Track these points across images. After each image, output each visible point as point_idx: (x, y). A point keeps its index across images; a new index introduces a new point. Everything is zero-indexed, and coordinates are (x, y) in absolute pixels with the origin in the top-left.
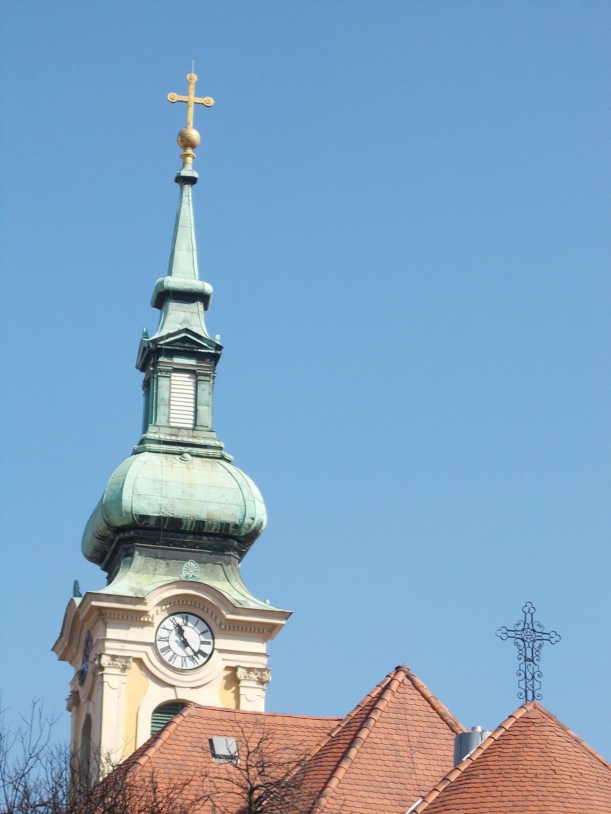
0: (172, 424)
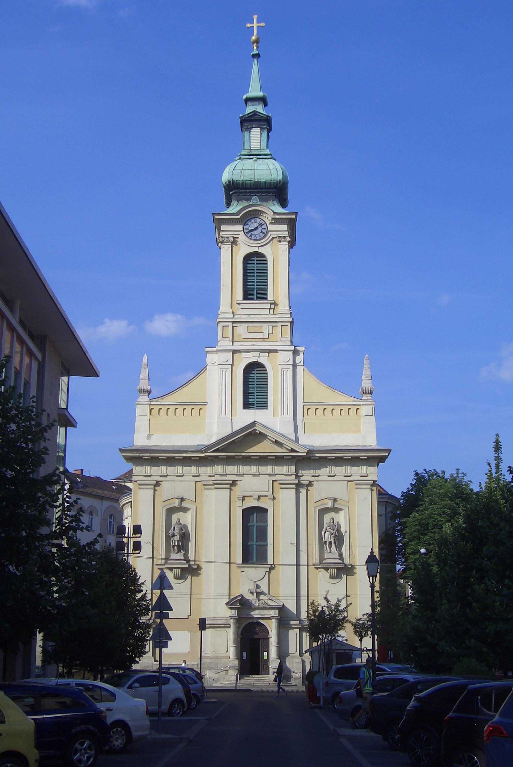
0: (251, 148)
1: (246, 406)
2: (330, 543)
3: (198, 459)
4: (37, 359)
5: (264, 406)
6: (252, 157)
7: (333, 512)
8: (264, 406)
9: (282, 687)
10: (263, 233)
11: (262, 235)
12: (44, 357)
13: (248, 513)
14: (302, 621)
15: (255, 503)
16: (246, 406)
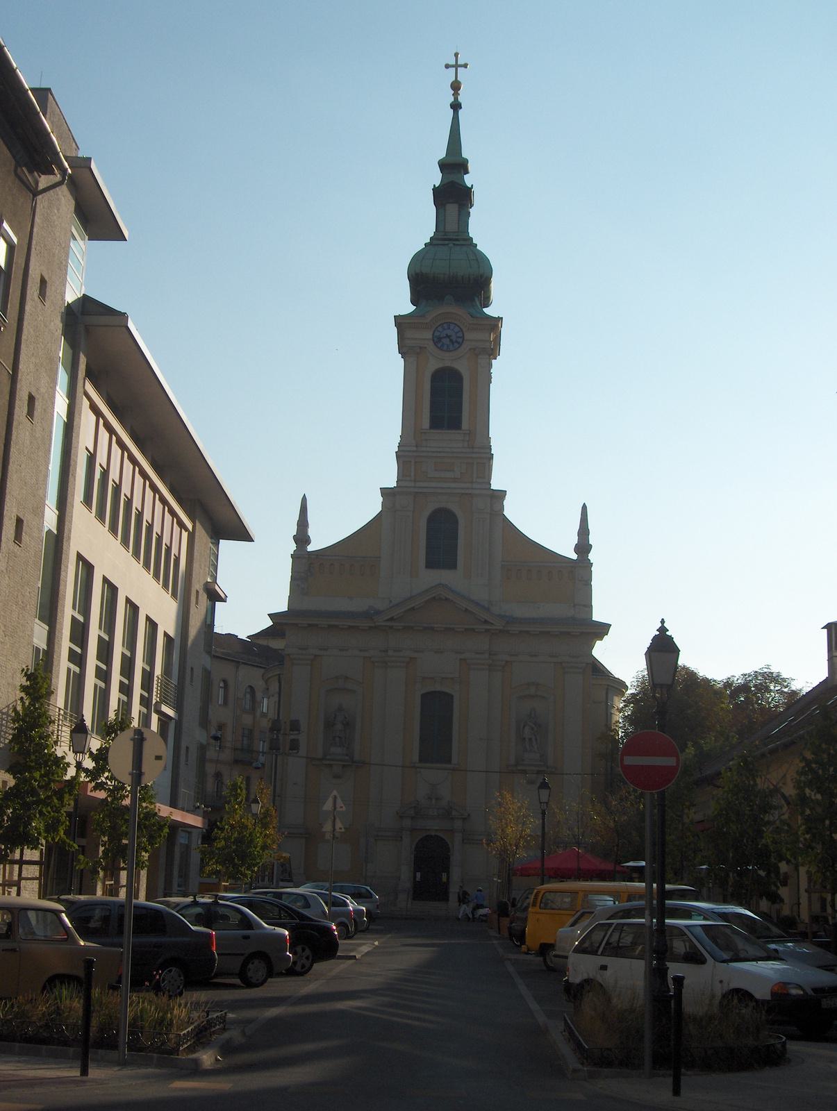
1: (430, 564)
2: (530, 739)
3: (55, 165)
4: (186, 529)
5: (453, 565)
6: (447, 242)
7: (505, 513)
8: (453, 565)
9: (547, 958)
10: (458, 343)
11: (452, 327)
12: (194, 527)
13: (428, 698)
14: (104, 320)
15: (438, 688)
16: (430, 564)
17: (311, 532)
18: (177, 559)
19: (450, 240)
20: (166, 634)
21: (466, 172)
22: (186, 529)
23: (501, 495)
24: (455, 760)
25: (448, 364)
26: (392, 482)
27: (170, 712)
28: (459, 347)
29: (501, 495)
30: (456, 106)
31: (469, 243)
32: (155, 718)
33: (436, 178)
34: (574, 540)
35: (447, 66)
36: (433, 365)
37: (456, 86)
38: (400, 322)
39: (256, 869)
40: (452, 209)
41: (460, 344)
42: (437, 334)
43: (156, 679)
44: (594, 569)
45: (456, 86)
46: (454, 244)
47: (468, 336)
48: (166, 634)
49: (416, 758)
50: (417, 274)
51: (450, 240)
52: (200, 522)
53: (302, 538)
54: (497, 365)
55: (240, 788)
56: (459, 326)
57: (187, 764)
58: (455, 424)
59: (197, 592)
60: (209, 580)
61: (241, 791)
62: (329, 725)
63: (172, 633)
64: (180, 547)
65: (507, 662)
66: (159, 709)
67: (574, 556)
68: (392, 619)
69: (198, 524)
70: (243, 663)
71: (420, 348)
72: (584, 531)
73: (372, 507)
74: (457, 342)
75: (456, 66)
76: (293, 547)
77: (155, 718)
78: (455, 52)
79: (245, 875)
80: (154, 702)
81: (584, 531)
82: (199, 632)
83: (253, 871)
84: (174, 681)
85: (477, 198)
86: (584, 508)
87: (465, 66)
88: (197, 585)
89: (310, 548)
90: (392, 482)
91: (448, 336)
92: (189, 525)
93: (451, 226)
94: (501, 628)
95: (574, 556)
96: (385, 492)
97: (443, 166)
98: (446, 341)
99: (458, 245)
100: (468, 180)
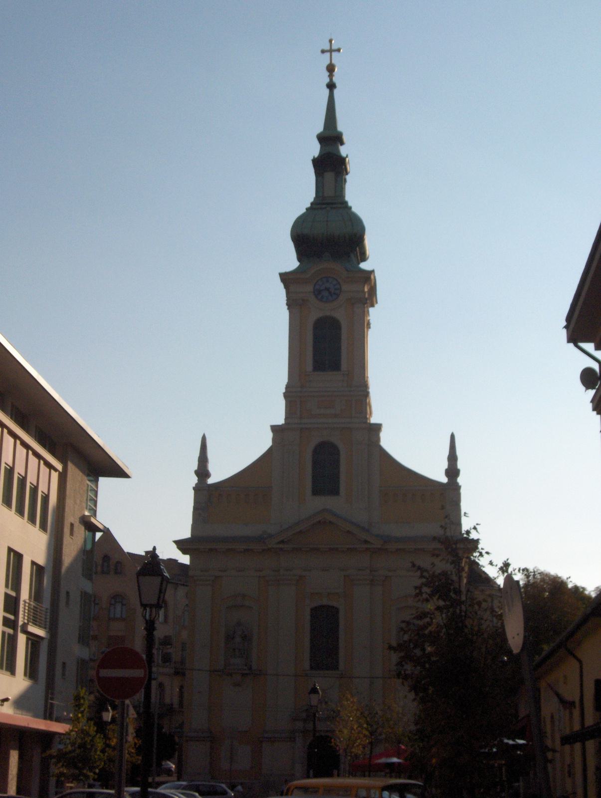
1: (316, 492)
4: (56, 470)
5: (335, 492)
6: (324, 206)
8: (335, 492)
15: (325, 602)
16: (316, 492)
17: (211, 467)
18: (46, 498)
19: (328, 204)
20: (33, 563)
21: (342, 143)
22: (56, 470)
23: (378, 428)
24: (341, 666)
25: (328, 314)
26: (280, 420)
27: (40, 632)
28: (337, 298)
29: (378, 428)
30: (331, 86)
31: (345, 206)
32: (22, 639)
33: (315, 149)
34: (445, 465)
35: (323, 52)
36: (314, 316)
37: (331, 69)
38: (286, 278)
39: (97, 771)
40: (329, 176)
41: (338, 295)
42: (317, 287)
43: (22, 603)
44: (462, 491)
45: (331, 69)
46: (331, 208)
47: (345, 287)
48: (33, 563)
49: (307, 665)
50: (298, 236)
51: (328, 204)
52: (73, 462)
53: (202, 472)
54: (374, 314)
55: (83, 698)
56: (318, 281)
57: (65, 679)
58: (335, 366)
59: (72, 525)
60: (87, 513)
61: (84, 701)
62: (229, 638)
63: (41, 561)
64: (48, 483)
65: (386, 577)
66: (25, 630)
67: (444, 480)
68: (282, 542)
69: (70, 466)
70: (181, 585)
71: (303, 300)
72: (453, 458)
73: (264, 442)
74: (335, 294)
75: (331, 51)
76: (195, 480)
77: (22, 639)
78: (330, 38)
79: (87, 777)
80: (20, 623)
81: (453, 458)
82: (76, 560)
83: (95, 773)
84: (46, 604)
85: (351, 166)
86: (453, 437)
87: (339, 50)
88: (71, 517)
89: (210, 481)
90: (280, 420)
91: (327, 289)
92: (59, 466)
93: (329, 192)
94: (379, 546)
95: (444, 480)
96: (275, 429)
97: (322, 138)
98: (326, 294)
99: (334, 208)
100: (343, 151)
